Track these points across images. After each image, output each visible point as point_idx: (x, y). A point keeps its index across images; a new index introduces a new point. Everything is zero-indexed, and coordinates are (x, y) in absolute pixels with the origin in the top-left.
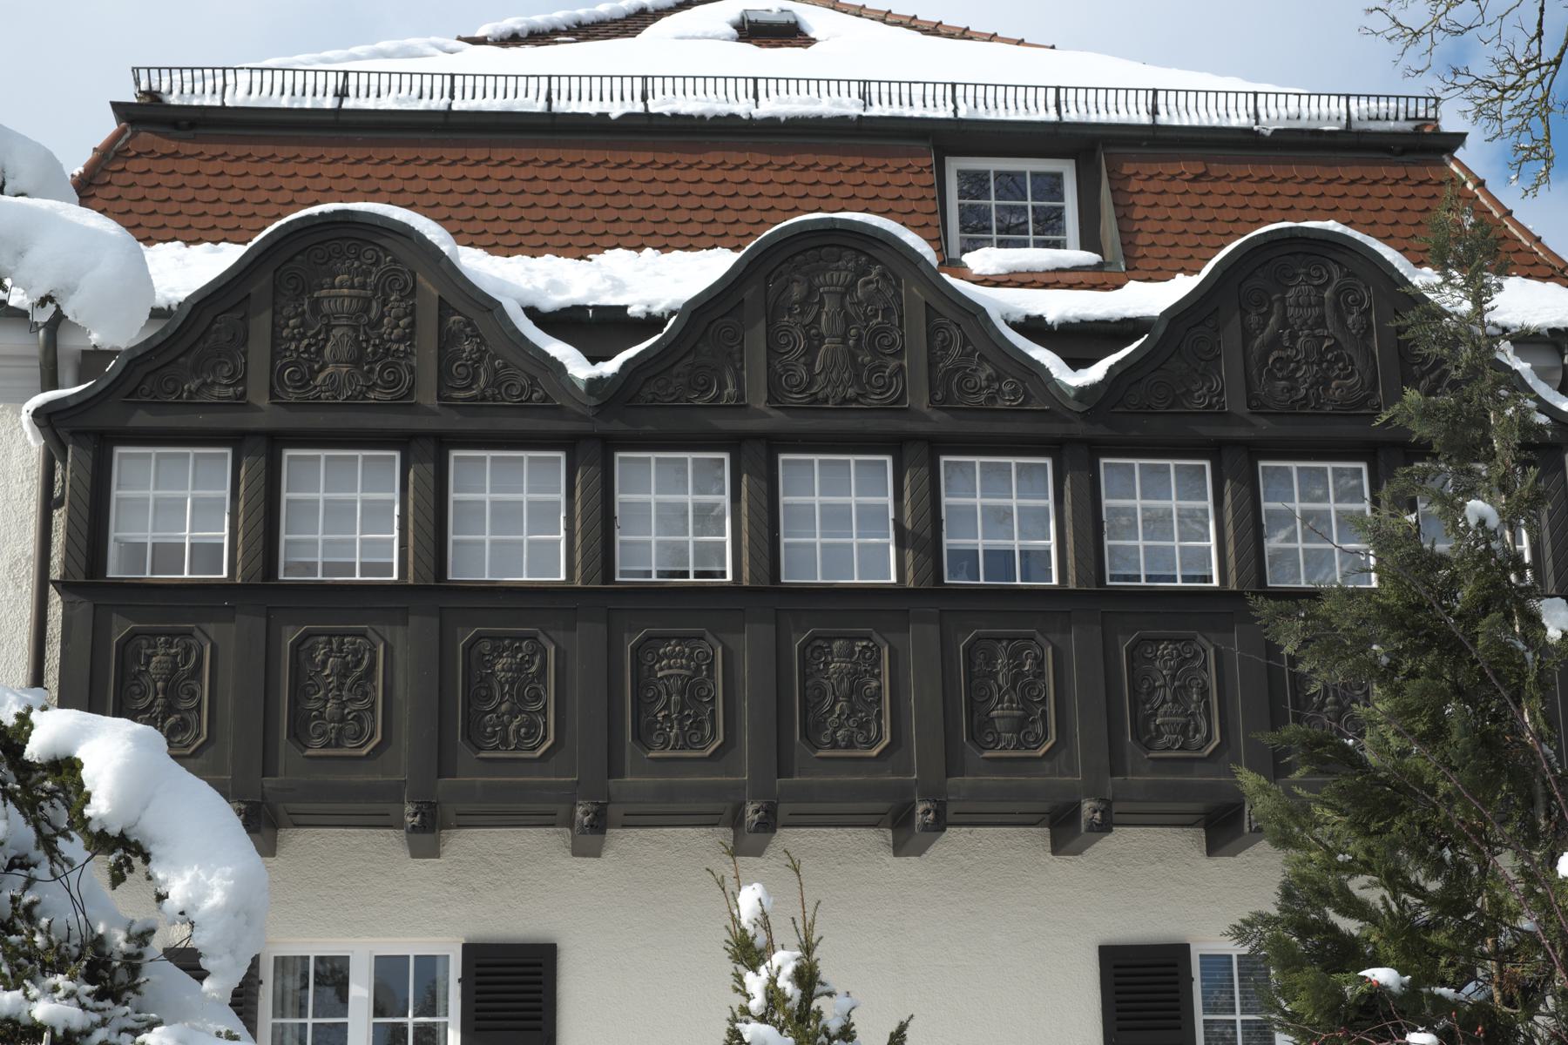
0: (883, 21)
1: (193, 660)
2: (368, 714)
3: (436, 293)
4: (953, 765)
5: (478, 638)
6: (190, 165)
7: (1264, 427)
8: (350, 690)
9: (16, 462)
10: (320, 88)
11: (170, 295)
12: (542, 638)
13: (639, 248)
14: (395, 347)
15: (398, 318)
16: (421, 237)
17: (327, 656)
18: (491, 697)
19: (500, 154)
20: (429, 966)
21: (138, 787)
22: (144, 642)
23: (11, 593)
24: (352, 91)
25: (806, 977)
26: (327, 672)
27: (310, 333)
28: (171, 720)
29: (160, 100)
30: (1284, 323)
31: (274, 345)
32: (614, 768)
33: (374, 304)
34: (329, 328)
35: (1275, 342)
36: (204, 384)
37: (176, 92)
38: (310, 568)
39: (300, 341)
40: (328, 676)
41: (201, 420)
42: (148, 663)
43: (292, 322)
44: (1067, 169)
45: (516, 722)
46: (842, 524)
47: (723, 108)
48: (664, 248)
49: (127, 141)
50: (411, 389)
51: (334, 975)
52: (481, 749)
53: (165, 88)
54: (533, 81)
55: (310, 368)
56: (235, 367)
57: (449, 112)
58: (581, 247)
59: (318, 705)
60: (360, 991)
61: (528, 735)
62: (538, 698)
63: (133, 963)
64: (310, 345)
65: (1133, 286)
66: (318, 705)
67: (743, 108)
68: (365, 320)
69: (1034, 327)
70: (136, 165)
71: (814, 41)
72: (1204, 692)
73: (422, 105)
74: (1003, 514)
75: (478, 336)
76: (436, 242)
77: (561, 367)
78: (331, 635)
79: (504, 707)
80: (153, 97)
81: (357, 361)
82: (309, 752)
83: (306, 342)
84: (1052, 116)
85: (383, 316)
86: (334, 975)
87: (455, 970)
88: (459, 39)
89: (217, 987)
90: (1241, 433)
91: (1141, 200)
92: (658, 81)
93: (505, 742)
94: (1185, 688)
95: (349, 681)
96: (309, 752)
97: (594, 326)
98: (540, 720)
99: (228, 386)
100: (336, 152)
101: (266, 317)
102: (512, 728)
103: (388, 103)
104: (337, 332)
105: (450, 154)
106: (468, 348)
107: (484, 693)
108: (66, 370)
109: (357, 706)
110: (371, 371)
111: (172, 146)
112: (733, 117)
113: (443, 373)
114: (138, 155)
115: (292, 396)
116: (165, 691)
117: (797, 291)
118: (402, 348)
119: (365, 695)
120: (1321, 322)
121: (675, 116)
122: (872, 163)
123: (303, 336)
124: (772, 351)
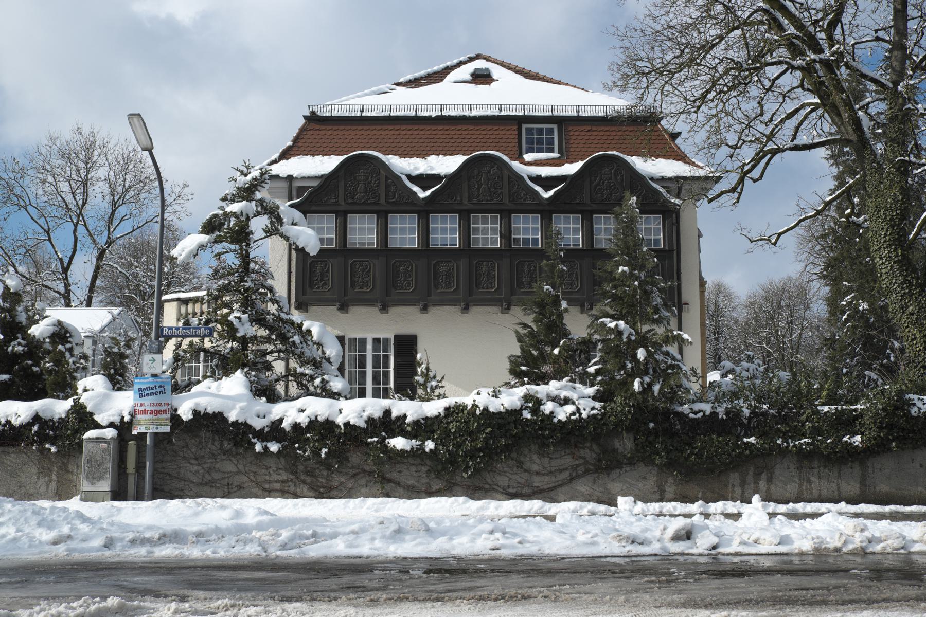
4: (513, 293)
6: (323, 132)
7: (595, 207)
13: (438, 155)
19: (403, 127)
20: (387, 340)
21: (322, 334)
25: (427, 369)
30: (601, 179)
32: (429, 294)
35: (598, 184)
41: (328, 208)
44: (555, 127)
46: (488, 233)
47: (462, 114)
48: (445, 155)
51: (363, 341)
58: (423, 155)
60: (369, 347)
63: (321, 362)
65: (567, 165)
67: (467, 113)
69: (537, 179)
70: (310, 133)
71: (493, 80)
72: (577, 275)
73: (382, 114)
74: (528, 229)
77: (415, 194)
81: (365, 192)
84: (550, 114)
86: (363, 341)
87: (392, 342)
89: (334, 367)
90: (589, 208)
91: (573, 138)
94: (572, 274)
97: (424, 180)
100: (360, 128)
101: (343, 182)
105: (390, 127)
108: (294, 193)
112: (464, 116)
113: (387, 195)
115: (350, 201)
117: (476, 172)
120: (611, 179)
122: (501, 128)
124: (469, 188)
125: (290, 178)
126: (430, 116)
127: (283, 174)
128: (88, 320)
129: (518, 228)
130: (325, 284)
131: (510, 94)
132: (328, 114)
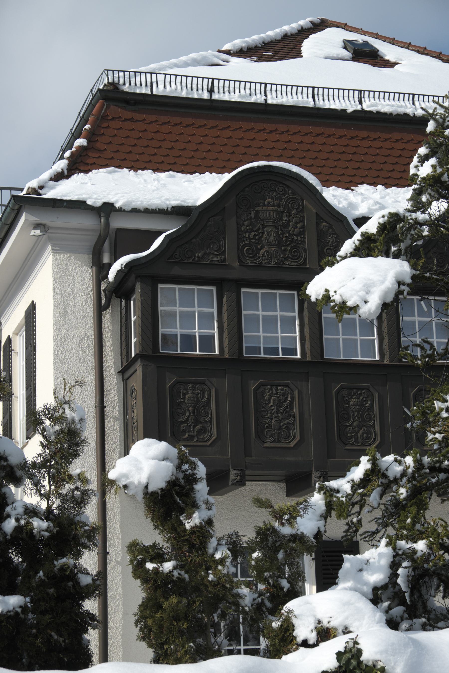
0: (408, 48)
1: (206, 397)
2: (292, 426)
3: (314, 211)
5: (342, 388)
8: (282, 414)
9: (78, 285)
10: (200, 86)
11: (168, 202)
12: (371, 389)
13: (374, 184)
14: (296, 238)
15: (297, 223)
16: (307, 182)
17: (271, 396)
18: (349, 419)
19: (294, 128)
22: (182, 387)
23: (81, 355)
24: (216, 89)
26: (271, 404)
27: (255, 229)
28: (198, 427)
29: (117, 88)
31: (238, 234)
33: (285, 215)
34: (264, 226)
36: (205, 253)
37: (127, 85)
38: (257, 350)
39: (250, 233)
40: (272, 406)
42: (184, 398)
43: (246, 223)
45: (361, 431)
49: (106, 110)
50: (305, 260)
52: (346, 445)
53: (121, 81)
54: (305, 89)
55: (256, 247)
56: (220, 245)
57: (266, 105)
59: (268, 420)
61: (368, 438)
62: (371, 419)
64: (255, 235)
66: (268, 420)
68: (280, 223)
73: (253, 100)
75: (335, 234)
76: (314, 184)
78: (272, 386)
79: (355, 424)
80: (114, 86)
81: (278, 245)
82: (266, 445)
83: (253, 234)
85: (289, 221)
88: (219, 51)
92: (366, 93)
93: (357, 441)
95: (282, 409)
96: (266, 445)
98: (372, 430)
99: (217, 255)
102: (360, 434)
103: (235, 97)
104: (268, 229)
106: (331, 240)
107: (346, 416)
109: (286, 422)
110: (285, 250)
111: (129, 115)
114: (113, 119)
115: (249, 262)
116: (194, 412)
118: (299, 238)
119: (290, 416)
121: (378, 113)
123: (252, 230)
125: (108, 208)
126: (344, 111)
127: (95, 199)
128: (335, 507)
129: (173, 315)
130: (203, 431)
131: (320, 75)
132: (146, 91)
